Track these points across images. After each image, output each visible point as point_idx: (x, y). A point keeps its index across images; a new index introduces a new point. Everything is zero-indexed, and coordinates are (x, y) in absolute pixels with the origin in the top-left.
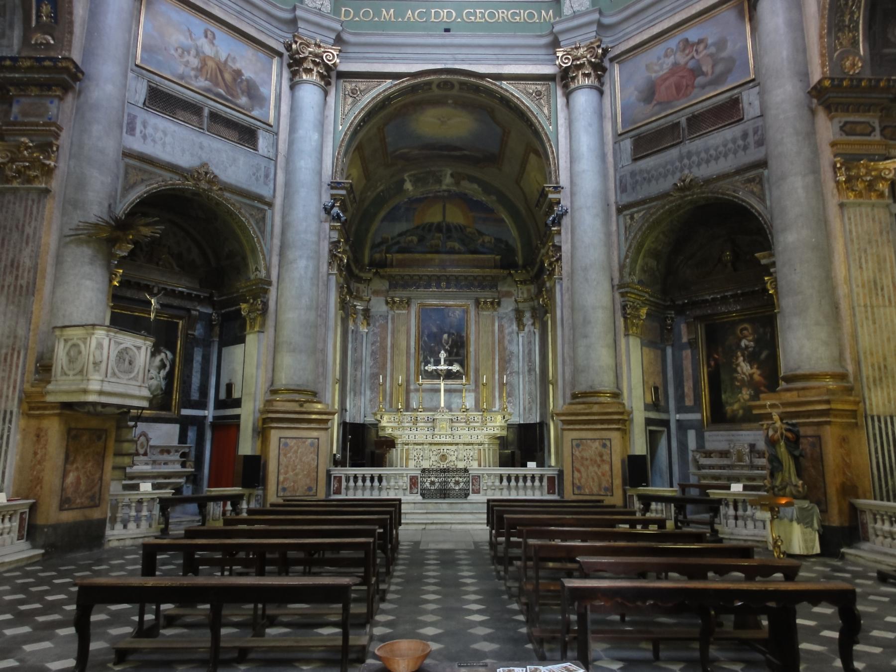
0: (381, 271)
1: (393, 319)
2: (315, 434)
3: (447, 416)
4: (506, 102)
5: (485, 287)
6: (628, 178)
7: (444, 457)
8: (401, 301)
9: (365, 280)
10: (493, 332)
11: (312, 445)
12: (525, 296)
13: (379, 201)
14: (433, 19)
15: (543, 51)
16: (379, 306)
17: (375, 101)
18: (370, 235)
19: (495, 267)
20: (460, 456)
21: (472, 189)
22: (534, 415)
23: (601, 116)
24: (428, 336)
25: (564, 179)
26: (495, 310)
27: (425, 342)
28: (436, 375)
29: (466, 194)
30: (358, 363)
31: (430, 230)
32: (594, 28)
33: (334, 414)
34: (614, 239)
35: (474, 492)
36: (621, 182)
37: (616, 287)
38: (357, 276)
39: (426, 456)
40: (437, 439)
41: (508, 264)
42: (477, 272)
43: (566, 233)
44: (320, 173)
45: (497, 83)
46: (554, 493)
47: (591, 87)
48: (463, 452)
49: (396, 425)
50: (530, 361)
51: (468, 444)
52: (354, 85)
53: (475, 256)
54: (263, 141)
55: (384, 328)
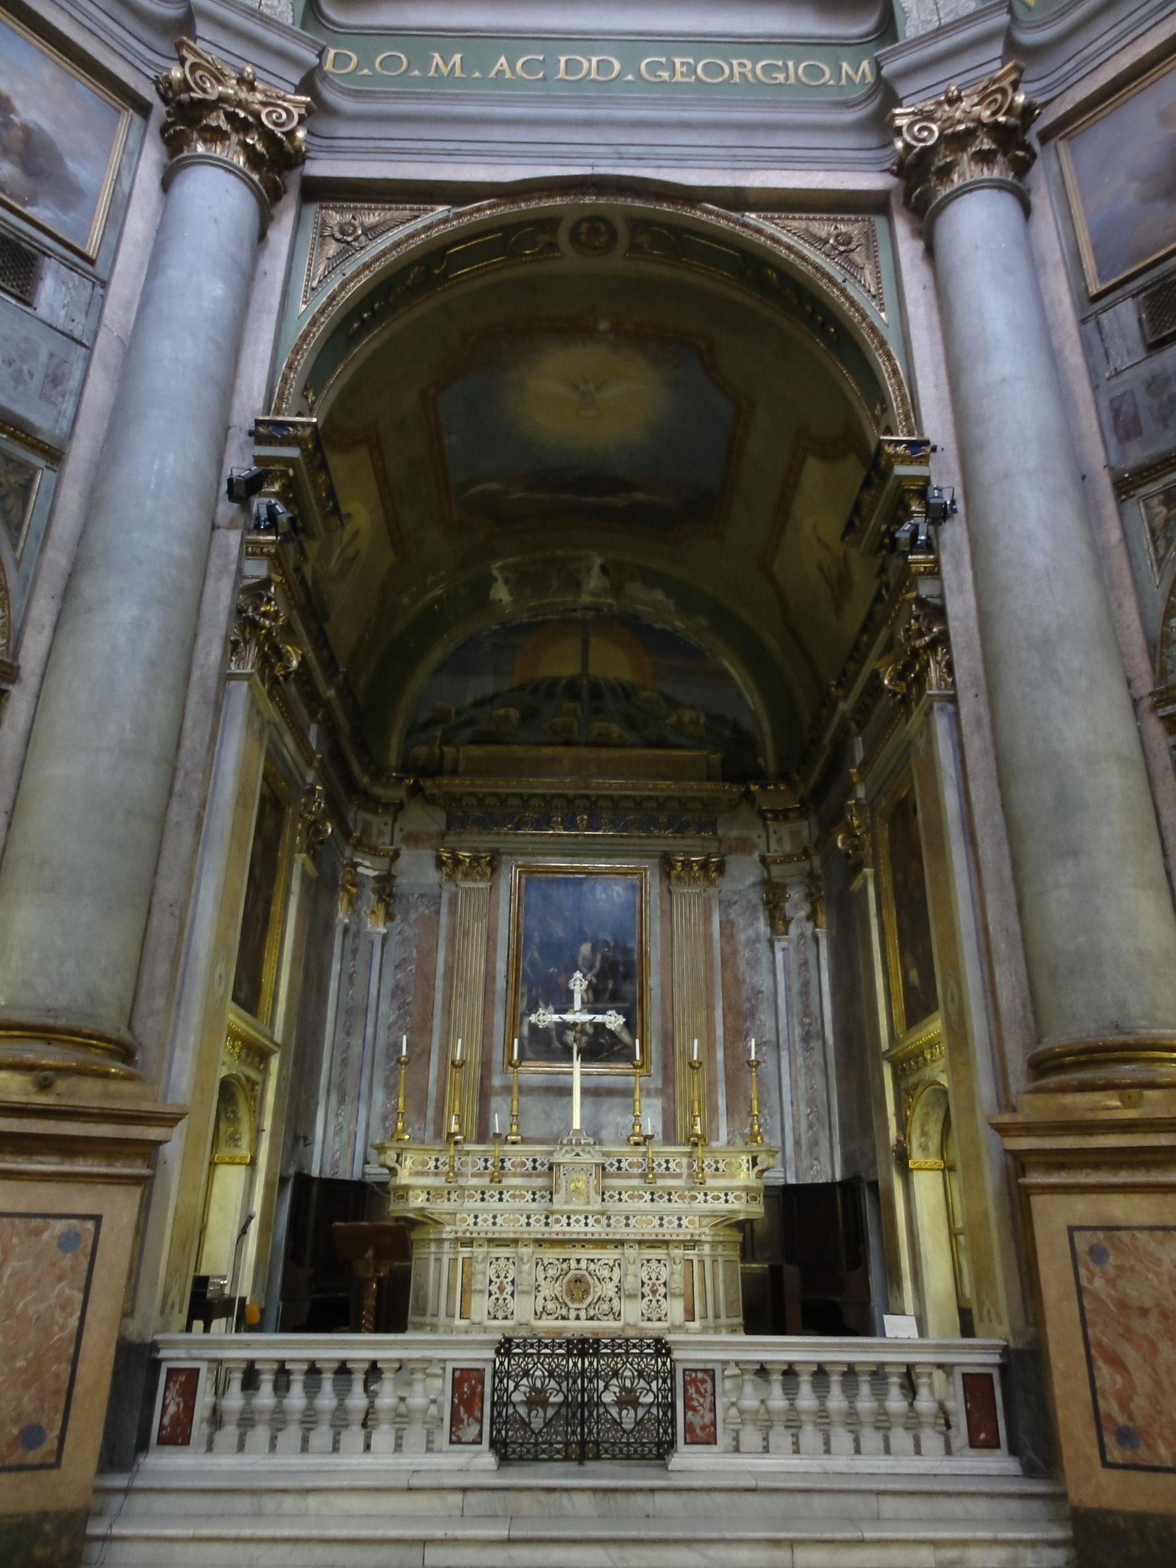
0: (426, 783)
1: (453, 903)
2: (82, 1200)
3: (591, 1158)
4: (759, 270)
5: (679, 826)
6: (1141, 397)
7: (578, 1287)
8: (476, 859)
9: (386, 806)
11: (68, 1242)
14: (562, 75)
15: (852, 141)
16: (418, 871)
17: (403, 249)
19: (709, 778)
20: (630, 1284)
21: (649, 601)
22: (825, 1159)
23: (1035, 265)
24: (544, 948)
25: (936, 423)
26: (712, 882)
27: (532, 963)
28: (549, 1045)
30: (352, 1014)
32: (997, 49)
33: (170, 1120)
34: (1119, 562)
35: (693, 1439)
36: (1116, 413)
37: (1146, 703)
38: (365, 793)
39: (526, 1282)
40: (559, 1229)
41: (739, 766)
42: (666, 787)
43: (957, 565)
44: (227, 389)
45: (734, 215)
47: (999, 186)
48: (637, 1268)
49: (440, 1182)
50: (806, 1013)
51: (653, 1244)
52: (348, 217)
54: (54, 290)
55: (431, 925)
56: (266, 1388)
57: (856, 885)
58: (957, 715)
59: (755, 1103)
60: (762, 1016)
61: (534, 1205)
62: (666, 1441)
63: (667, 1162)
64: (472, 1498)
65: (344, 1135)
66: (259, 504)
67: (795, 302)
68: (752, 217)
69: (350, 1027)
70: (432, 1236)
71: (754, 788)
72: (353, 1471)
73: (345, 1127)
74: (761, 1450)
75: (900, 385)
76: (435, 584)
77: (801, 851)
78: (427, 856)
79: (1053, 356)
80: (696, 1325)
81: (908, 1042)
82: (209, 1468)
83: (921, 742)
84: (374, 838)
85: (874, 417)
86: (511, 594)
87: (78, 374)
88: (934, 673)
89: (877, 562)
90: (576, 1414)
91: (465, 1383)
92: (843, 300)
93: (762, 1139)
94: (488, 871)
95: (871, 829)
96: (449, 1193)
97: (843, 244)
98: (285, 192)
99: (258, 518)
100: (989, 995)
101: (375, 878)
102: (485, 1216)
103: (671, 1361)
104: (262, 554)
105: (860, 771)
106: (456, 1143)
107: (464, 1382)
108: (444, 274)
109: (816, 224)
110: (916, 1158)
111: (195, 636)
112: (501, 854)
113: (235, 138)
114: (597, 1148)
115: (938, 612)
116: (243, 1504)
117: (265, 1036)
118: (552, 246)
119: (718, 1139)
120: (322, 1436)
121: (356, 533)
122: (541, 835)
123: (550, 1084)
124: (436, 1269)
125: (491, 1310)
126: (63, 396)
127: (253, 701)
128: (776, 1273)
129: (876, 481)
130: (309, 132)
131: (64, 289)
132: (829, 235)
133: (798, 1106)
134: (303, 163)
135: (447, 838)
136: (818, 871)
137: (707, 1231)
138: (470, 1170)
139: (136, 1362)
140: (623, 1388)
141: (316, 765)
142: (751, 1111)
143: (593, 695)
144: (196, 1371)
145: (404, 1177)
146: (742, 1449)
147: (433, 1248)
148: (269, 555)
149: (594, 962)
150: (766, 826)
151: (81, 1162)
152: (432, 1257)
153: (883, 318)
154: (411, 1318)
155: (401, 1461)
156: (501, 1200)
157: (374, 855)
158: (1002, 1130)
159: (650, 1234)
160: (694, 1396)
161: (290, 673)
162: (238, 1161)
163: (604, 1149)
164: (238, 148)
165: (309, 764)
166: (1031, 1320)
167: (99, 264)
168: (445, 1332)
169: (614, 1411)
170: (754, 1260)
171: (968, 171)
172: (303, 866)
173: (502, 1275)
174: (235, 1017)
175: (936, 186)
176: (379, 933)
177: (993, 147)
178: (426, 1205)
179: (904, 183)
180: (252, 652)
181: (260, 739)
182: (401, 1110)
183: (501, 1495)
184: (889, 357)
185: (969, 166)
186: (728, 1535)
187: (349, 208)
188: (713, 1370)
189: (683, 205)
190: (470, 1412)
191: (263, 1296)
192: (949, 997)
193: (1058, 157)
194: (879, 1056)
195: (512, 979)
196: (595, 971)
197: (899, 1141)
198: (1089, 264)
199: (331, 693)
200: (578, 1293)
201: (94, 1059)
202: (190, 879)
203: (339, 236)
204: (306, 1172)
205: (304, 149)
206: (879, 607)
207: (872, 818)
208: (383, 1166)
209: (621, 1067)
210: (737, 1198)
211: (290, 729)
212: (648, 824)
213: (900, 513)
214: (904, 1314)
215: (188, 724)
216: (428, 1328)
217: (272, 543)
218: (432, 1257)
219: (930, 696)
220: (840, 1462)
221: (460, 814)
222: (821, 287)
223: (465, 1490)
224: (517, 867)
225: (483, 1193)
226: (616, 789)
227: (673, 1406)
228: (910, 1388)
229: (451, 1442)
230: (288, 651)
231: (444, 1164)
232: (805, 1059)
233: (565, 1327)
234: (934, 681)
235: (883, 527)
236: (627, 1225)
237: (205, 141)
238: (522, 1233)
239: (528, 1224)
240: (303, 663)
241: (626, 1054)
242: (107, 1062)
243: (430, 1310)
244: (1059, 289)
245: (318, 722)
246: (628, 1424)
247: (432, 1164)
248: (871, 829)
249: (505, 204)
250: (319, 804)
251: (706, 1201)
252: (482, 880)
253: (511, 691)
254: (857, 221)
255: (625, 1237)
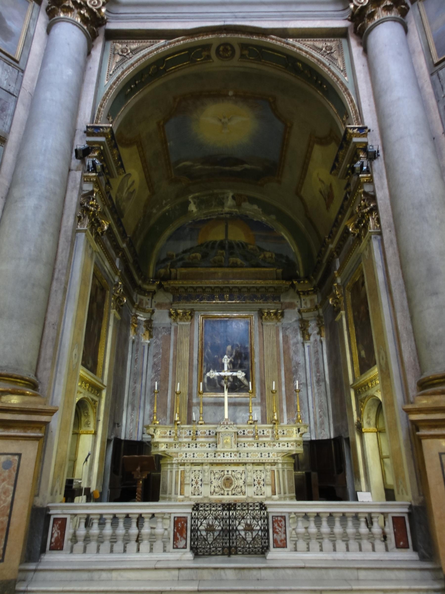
0: (164, 283)
2: (13, 447)
5: (265, 298)
7: (228, 482)
8: (185, 313)
9: (149, 292)
10: (278, 342)
11: (7, 465)
12: (309, 306)
13: (165, 221)
16: (162, 318)
18: (155, 251)
19: (277, 279)
20: (249, 480)
21: (251, 210)
22: (327, 430)
23: (410, 53)
24: (211, 348)
25: (370, 120)
26: (279, 320)
27: (208, 354)
28: (215, 386)
29: (247, 216)
30: (137, 375)
31: (213, 248)
33: (51, 413)
35: (277, 545)
38: (140, 287)
40: (220, 458)
41: (289, 273)
42: (260, 283)
43: (380, 178)
45: (283, 40)
46: (406, 546)
47: (395, 20)
48: (252, 474)
49: (171, 440)
50: (318, 371)
51: (259, 464)
52: (125, 46)
53: (257, 269)
55: (167, 339)
56: (96, 526)
57: (337, 319)
58: (382, 241)
59: (298, 406)
60: (300, 373)
61: (210, 449)
62: (265, 547)
63: (263, 431)
64: (183, 572)
65: (134, 423)
66: (89, 161)
67: (309, 76)
68: (291, 41)
69: (136, 380)
70: (169, 462)
71: (295, 282)
72: (132, 561)
73: (134, 420)
74: (306, 549)
75: (354, 106)
76: (166, 204)
77: (314, 307)
78: (166, 312)
79: (420, 89)
80: (276, 497)
81: (361, 380)
82: (71, 560)
83: (366, 253)
84: (144, 305)
85: (343, 121)
86: (197, 208)
87: (12, 108)
88: (371, 223)
89: (345, 182)
90: (227, 535)
91: (179, 524)
92: (329, 72)
93: (302, 421)
94: (190, 317)
95: (344, 295)
96: (175, 445)
97: (329, 50)
98: (98, 36)
99: (89, 166)
100: (399, 356)
101: (145, 321)
102: (190, 454)
103: (267, 512)
104: (90, 181)
105: (339, 271)
106: (178, 425)
107: (179, 522)
108: (165, 69)
109: (318, 43)
110: (365, 427)
111: (62, 214)
112: (194, 311)
113: (76, 11)
114: (235, 425)
115: (373, 198)
116: (85, 575)
117: (100, 383)
118: (209, 57)
119: (283, 422)
120: (119, 546)
121: (133, 182)
122: (210, 303)
123: (216, 402)
124: (170, 476)
125: (193, 492)
126: (6, 116)
127: (87, 242)
128: (308, 475)
129: (345, 145)
130: (107, 11)
131: (6, 73)
132: (323, 47)
133: (315, 409)
134: (106, 24)
135: (173, 305)
136: (321, 314)
137: (280, 458)
138: (183, 435)
139: (39, 517)
140: (246, 524)
141: (119, 274)
142: (297, 409)
143: (230, 247)
144: (65, 519)
145: (157, 439)
146: (298, 549)
147: (169, 467)
148: (93, 181)
149: (232, 353)
150: (300, 298)
151: (12, 431)
152: (169, 471)
153: (346, 80)
154: (161, 495)
155: (153, 556)
156: (196, 447)
157: (144, 312)
158: (408, 412)
159: (257, 460)
160: (277, 527)
161: (104, 231)
162: (89, 432)
163: (238, 426)
164: (78, 15)
165: (116, 274)
166: (421, 494)
167: (20, 63)
168: (175, 501)
169: (243, 533)
170: (299, 470)
171: (381, 14)
172: (114, 315)
173: (197, 477)
174: (82, 372)
175: (367, 22)
176: (146, 343)
177: (392, 4)
178: (166, 449)
179: (353, 24)
180: (87, 221)
181: (92, 257)
182: (155, 411)
183: (195, 571)
184: (349, 95)
185: (382, 13)
186: (293, 588)
187: (125, 43)
188: (285, 517)
189: (262, 37)
190: (181, 535)
191: (101, 487)
192: (381, 358)
193: (419, 8)
194: (348, 386)
195: (200, 360)
196: (233, 356)
197: (358, 421)
198: (433, 50)
199: (124, 245)
200: (228, 484)
201: (19, 387)
202: (61, 313)
203: (121, 53)
204: (119, 437)
205: (105, 18)
206: (346, 203)
207: (344, 290)
208: (149, 434)
209: (244, 394)
210: (292, 445)
211: (107, 259)
212: (253, 298)
213: (355, 159)
214: (361, 491)
215: (60, 250)
216: (168, 499)
217: (94, 176)
218: (169, 471)
219: (370, 232)
220: (340, 555)
221: (178, 295)
222: (320, 68)
223: (179, 569)
224: (201, 316)
225: (189, 444)
226: (240, 284)
227: (268, 531)
228: (369, 522)
229: (174, 548)
230: (103, 223)
231: (173, 433)
232: (318, 390)
233: (223, 498)
234: (372, 226)
235: (348, 166)
236: (248, 456)
237: (64, 12)
238: (205, 460)
239: (207, 457)
240: (110, 227)
241: (245, 389)
242: (24, 389)
243: (168, 492)
244: (421, 62)
245: (119, 257)
246: (249, 539)
247: (168, 433)
248: (344, 295)
249: (189, 39)
250: (120, 290)
251: (279, 446)
252: (187, 321)
253: (198, 246)
254: (334, 41)
255: (247, 461)
